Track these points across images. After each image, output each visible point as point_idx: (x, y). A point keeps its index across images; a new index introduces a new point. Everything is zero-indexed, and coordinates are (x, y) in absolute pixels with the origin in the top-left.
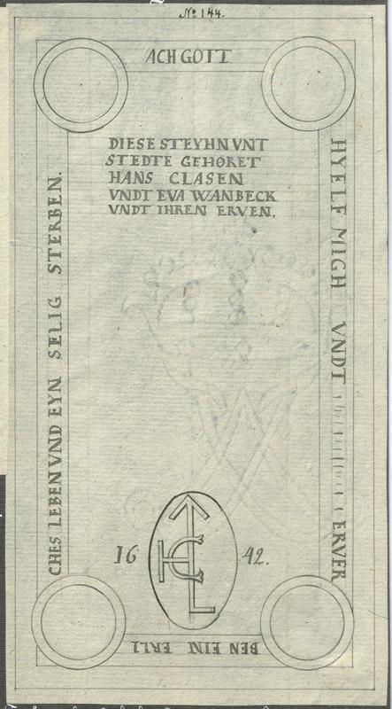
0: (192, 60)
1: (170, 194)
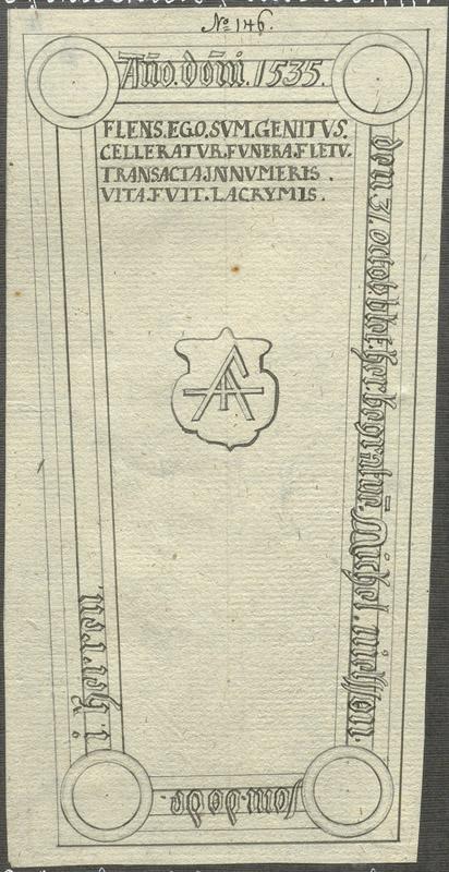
0: (271, 134)
1: (241, 150)
